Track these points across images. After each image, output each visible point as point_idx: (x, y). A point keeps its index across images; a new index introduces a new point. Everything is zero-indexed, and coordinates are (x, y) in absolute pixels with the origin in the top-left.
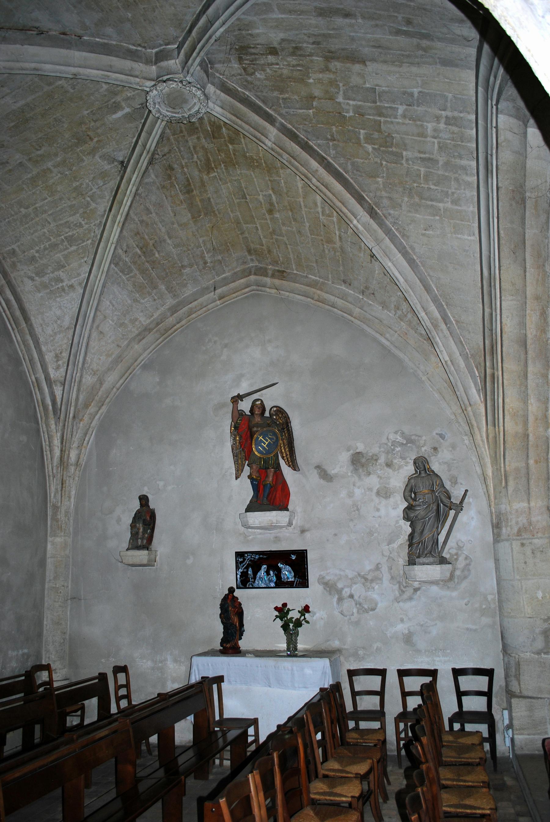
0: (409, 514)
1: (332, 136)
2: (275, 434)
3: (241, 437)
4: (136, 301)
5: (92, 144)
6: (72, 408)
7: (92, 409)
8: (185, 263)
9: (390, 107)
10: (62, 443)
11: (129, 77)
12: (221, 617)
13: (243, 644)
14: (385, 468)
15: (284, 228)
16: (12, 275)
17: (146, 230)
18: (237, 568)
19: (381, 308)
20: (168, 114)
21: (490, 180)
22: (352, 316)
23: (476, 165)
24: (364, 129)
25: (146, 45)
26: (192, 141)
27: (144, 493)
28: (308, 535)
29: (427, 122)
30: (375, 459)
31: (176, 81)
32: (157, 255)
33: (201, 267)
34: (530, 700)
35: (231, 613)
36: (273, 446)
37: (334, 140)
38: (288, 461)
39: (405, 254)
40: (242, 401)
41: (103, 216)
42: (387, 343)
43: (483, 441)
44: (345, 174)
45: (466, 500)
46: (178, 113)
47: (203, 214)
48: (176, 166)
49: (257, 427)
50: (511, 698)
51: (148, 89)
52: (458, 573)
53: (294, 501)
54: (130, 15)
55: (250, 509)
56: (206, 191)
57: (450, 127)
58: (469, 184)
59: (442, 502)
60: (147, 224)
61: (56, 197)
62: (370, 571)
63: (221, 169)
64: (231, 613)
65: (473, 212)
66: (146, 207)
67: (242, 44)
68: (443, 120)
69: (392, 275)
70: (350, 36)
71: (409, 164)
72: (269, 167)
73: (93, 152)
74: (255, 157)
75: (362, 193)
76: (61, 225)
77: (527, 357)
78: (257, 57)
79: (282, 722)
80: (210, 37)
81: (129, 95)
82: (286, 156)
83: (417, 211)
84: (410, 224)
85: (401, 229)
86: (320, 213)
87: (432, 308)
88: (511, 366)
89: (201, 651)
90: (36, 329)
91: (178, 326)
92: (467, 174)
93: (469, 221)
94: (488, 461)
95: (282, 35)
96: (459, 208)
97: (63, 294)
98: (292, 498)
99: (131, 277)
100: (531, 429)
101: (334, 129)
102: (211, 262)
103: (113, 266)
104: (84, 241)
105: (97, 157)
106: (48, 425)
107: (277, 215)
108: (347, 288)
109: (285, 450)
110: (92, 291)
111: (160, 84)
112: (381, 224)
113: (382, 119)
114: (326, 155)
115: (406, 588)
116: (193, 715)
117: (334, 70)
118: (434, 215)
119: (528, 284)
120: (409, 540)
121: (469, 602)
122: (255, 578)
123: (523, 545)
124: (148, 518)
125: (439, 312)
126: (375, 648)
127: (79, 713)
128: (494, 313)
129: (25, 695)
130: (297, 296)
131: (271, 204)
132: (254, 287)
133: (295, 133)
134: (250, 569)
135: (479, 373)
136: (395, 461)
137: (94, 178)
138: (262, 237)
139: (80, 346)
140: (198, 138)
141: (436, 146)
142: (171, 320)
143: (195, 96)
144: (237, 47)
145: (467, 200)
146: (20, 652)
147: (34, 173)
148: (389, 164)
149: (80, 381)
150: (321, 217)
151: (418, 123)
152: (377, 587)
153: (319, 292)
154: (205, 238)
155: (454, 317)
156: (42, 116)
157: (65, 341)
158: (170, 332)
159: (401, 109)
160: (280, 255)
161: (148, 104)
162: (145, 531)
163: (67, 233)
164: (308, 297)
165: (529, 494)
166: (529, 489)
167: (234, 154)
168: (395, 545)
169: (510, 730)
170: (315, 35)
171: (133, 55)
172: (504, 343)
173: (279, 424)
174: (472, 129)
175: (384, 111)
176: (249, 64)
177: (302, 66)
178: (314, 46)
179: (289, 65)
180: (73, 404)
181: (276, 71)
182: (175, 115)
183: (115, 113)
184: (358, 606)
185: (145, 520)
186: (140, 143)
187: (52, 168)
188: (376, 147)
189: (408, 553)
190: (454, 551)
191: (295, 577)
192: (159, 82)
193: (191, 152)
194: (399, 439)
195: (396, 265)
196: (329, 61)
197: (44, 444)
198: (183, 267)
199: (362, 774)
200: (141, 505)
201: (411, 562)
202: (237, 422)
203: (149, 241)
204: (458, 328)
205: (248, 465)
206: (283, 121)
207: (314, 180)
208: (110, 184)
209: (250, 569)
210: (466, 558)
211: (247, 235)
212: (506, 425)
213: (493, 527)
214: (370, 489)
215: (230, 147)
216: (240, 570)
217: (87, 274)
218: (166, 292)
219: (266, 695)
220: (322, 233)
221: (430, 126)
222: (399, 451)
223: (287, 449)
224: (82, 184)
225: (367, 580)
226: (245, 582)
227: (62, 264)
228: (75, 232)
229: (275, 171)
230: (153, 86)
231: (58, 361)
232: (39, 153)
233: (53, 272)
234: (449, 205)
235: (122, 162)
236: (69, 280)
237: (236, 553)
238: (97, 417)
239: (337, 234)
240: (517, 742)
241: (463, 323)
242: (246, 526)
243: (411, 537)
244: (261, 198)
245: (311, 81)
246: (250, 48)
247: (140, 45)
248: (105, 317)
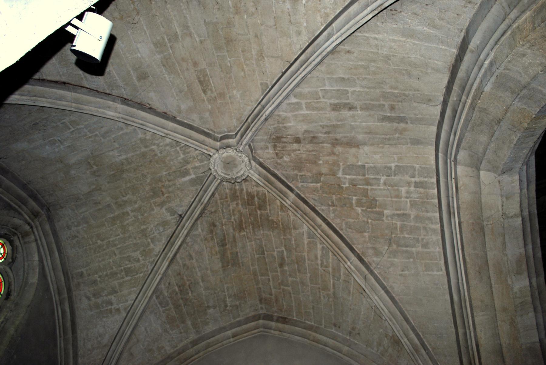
1: (333, 203)
4: (166, 331)
5: (163, 198)
8: (211, 304)
15: (290, 279)
16: (74, 293)
17: (186, 273)
24: (356, 196)
26: (233, 206)
29: (402, 187)
32: (190, 294)
33: (222, 310)
37: (334, 206)
41: (157, 256)
46: (229, 175)
47: (230, 264)
48: (218, 224)
56: (236, 246)
57: (418, 189)
58: (434, 231)
60: (188, 268)
61: (127, 235)
63: (250, 229)
65: (439, 252)
66: (189, 253)
67: (278, 135)
68: (413, 185)
70: (351, 125)
73: (162, 204)
76: (124, 258)
78: (286, 144)
81: (197, 165)
83: (395, 256)
84: (390, 267)
85: (382, 273)
90: (79, 342)
91: (196, 356)
92: (432, 223)
93: (436, 260)
95: (305, 127)
96: (428, 250)
97: (110, 315)
99: (166, 310)
101: (334, 197)
102: (231, 306)
104: (137, 274)
105: (164, 209)
107: (286, 268)
108: (337, 330)
110: (134, 313)
113: (369, 187)
117: (337, 153)
118: (409, 258)
119: (495, 298)
128: (468, 331)
130: (296, 337)
131: (283, 258)
132: (262, 329)
137: (158, 224)
138: (272, 287)
140: (237, 204)
141: (409, 204)
142: (191, 351)
145: (434, 243)
147: (116, 214)
148: (373, 222)
150: (320, 268)
151: (396, 188)
153: (314, 334)
154: (229, 285)
155: (430, 345)
156: (135, 170)
157: (100, 357)
160: (284, 303)
163: (126, 265)
167: (261, 218)
170: (327, 126)
174: (434, 189)
175: (371, 181)
177: (316, 151)
178: (326, 135)
179: (307, 151)
181: (297, 156)
183: (184, 177)
187: (130, 212)
188: (364, 209)
193: (230, 214)
196: (334, 147)
198: (208, 307)
203: (186, 281)
207: (319, 231)
208: (168, 231)
211: (261, 286)
215: (259, 212)
218: (191, 327)
220: (320, 282)
221: (403, 190)
224: (147, 228)
227: (116, 289)
228: (132, 265)
229: (288, 231)
232: (124, 199)
233: (107, 296)
234: (420, 249)
235: (180, 215)
236: (117, 304)
241: (439, 349)
244: (275, 254)
245: (321, 162)
246: (283, 137)
247: (211, 130)
248: (138, 341)
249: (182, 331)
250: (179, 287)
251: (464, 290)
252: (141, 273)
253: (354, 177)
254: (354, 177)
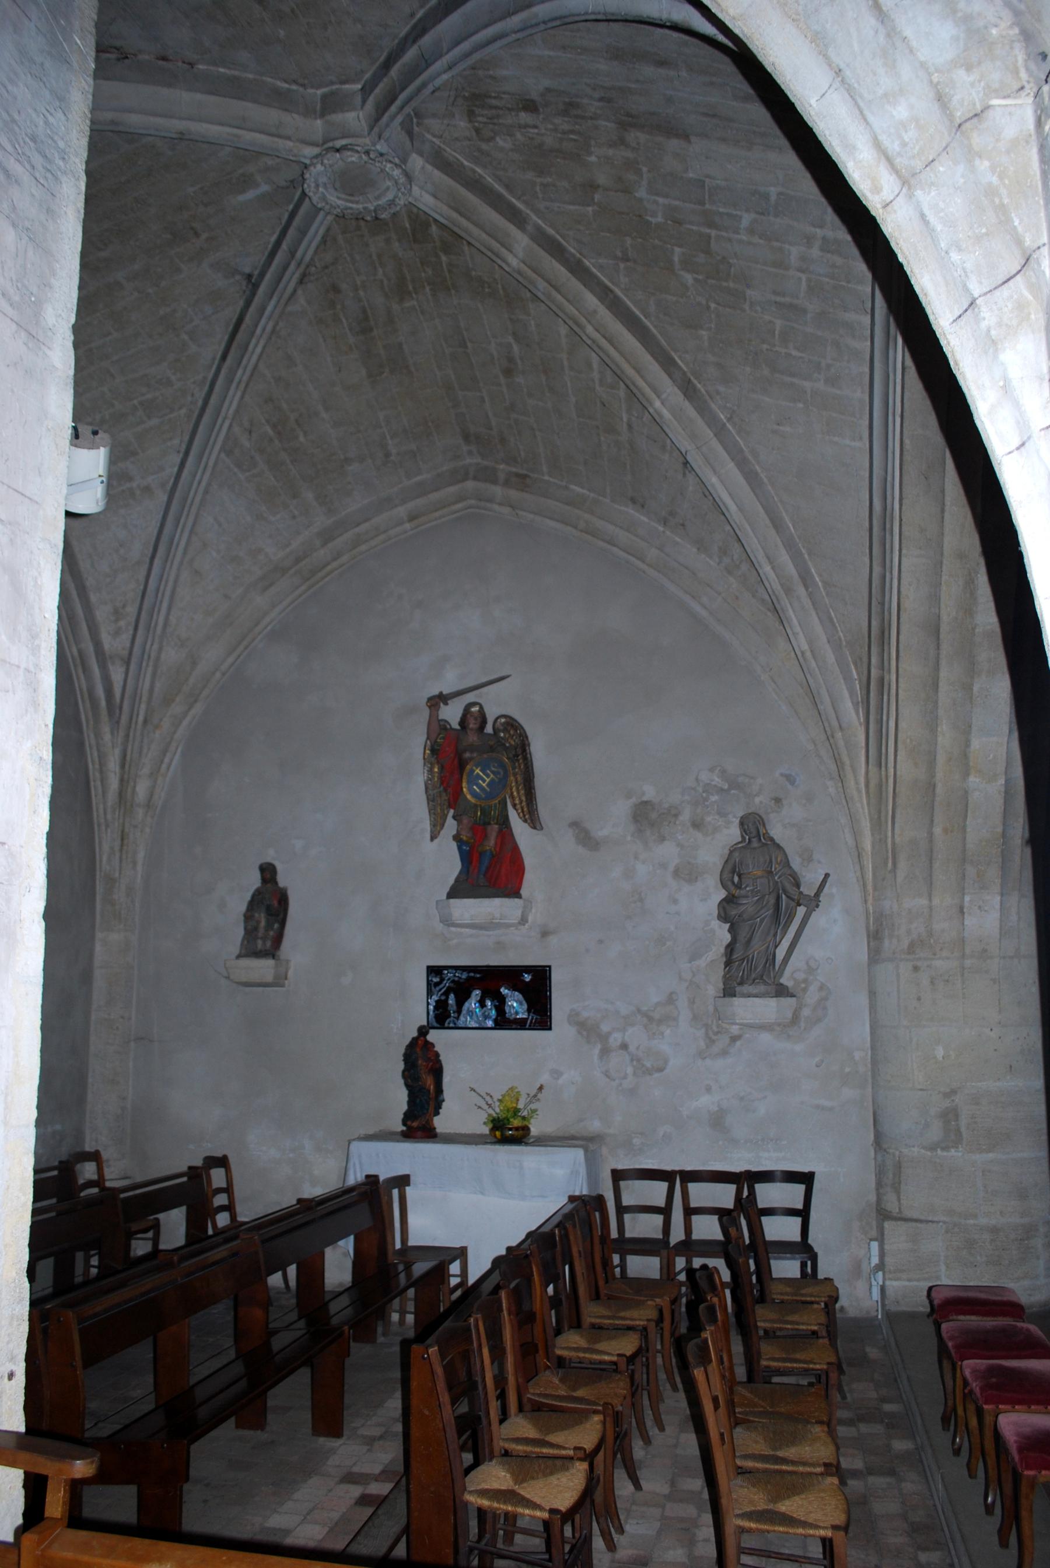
0: (727, 910)
2: (502, 765)
3: (442, 768)
6: (143, 706)
7: (177, 708)
9: (727, 214)
10: (123, 766)
11: (276, 139)
12: (404, 1076)
13: (441, 1123)
14: (691, 829)
18: (430, 993)
19: (695, 550)
20: (339, 202)
21: (891, 352)
22: (643, 562)
23: (869, 322)
24: (681, 246)
25: (306, 82)
27: (269, 860)
28: (553, 940)
30: (672, 813)
31: (358, 152)
32: (302, 439)
34: (914, 1224)
35: (423, 1072)
36: (500, 785)
37: (628, 260)
38: (523, 812)
39: (742, 463)
40: (446, 704)
42: (704, 613)
43: (859, 791)
44: (643, 318)
45: (826, 890)
46: (357, 202)
48: (344, 286)
49: (472, 752)
50: (883, 1221)
51: (308, 162)
52: (806, 1012)
53: (532, 881)
54: (282, 33)
55: (454, 893)
57: (829, 255)
59: (785, 891)
62: (658, 1004)
64: (423, 1072)
69: (717, 499)
71: (756, 312)
72: (510, 295)
74: (486, 279)
75: (673, 354)
77: (938, 654)
78: (501, 112)
79: (514, 1243)
80: (424, 85)
82: (542, 284)
86: (597, 382)
87: (784, 558)
88: (910, 669)
89: (362, 1132)
91: (335, 564)
94: (866, 825)
95: (546, 83)
96: (838, 392)
98: (528, 876)
100: (939, 775)
101: (629, 241)
103: (223, 455)
106: (98, 735)
109: (518, 793)
110: (185, 499)
111: (329, 155)
112: (703, 410)
113: (713, 233)
114: (613, 283)
115: (718, 1036)
116: (352, 1238)
120: (726, 954)
121: (822, 1061)
122: (459, 1011)
123: (916, 969)
124: (275, 903)
125: (796, 566)
126: (661, 1134)
127: (150, 1234)
128: (888, 574)
129: (58, 1202)
130: (548, 522)
131: (511, 360)
132: (473, 502)
133: (559, 244)
134: (452, 996)
135: (858, 674)
136: (709, 819)
138: (490, 415)
139: (160, 595)
140: (388, 241)
143: (390, 177)
144: (467, 94)
146: (50, 1130)
148: (720, 308)
149: (158, 659)
150: (597, 388)
151: (776, 244)
152: (668, 1032)
153: (587, 516)
155: (820, 575)
158: (320, 575)
159: (746, 219)
161: (305, 186)
162: (269, 926)
163: (143, 395)
164: (567, 524)
165: (931, 884)
166: (931, 876)
167: (450, 271)
168: (702, 963)
169: (880, 1273)
171: (282, 100)
172: (903, 628)
173: (511, 747)
176: (485, 123)
180: (144, 699)
181: (532, 139)
182: (350, 205)
184: (635, 1063)
185: (270, 907)
186: (284, 246)
188: (700, 277)
189: (724, 976)
190: (801, 976)
191: (529, 1011)
192: (328, 150)
194: (717, 780)
195: (725, 481)
196: (626, 130)
197: (90, 766)
198: (348, 461)
199: (563, 1509)
200: (264, 880)
201: (729, 992)
202: (436, 742)
204: (827, 595)
205: (454, 817)
206: (540, 222)
207: (590, 329)
209: (452, 996)
210: (822, 988)
212: (898, 767)
213: (868, 936)
214: (664, 866)
215: (444, 258)
216: (435, 998)
217: (176, 469)
219: (473, 1209)
221: (794, 252)
222: (715, 802)
223: (522, 792)
225: (653, 1020)
226: (442, 1017)
230: (316, 157)
231: (117, 620)
232: (103, 254)
235: (249, 276)
237: (428, 967)
238: (185, 723)
239: (625, 419)
240: (889, 1292)
242: (447, 921)
243: (730, 948)
245: (593, 159)
246: (490, 97)
247: (295, 82)
249: (296, 513)
250: (274, 427)
251: (893, 498)
252: (180, 408)
253: (677, 203)
254: (677, 203)
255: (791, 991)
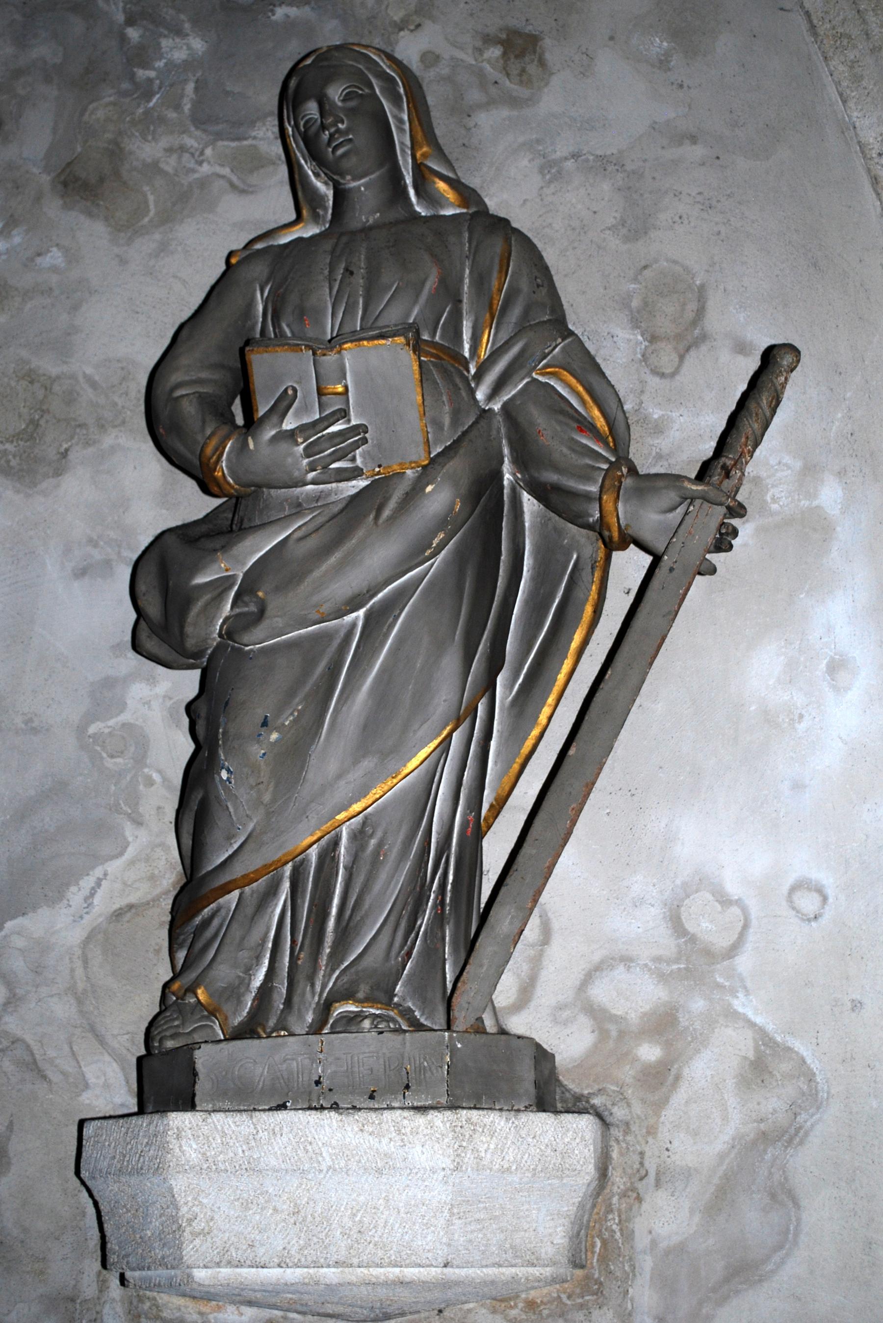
14: (52, 207)
136: (146, 150)
190: (633, 995)
210: (763, 1064)
222: (188, 65)
255: (571, 1084)
